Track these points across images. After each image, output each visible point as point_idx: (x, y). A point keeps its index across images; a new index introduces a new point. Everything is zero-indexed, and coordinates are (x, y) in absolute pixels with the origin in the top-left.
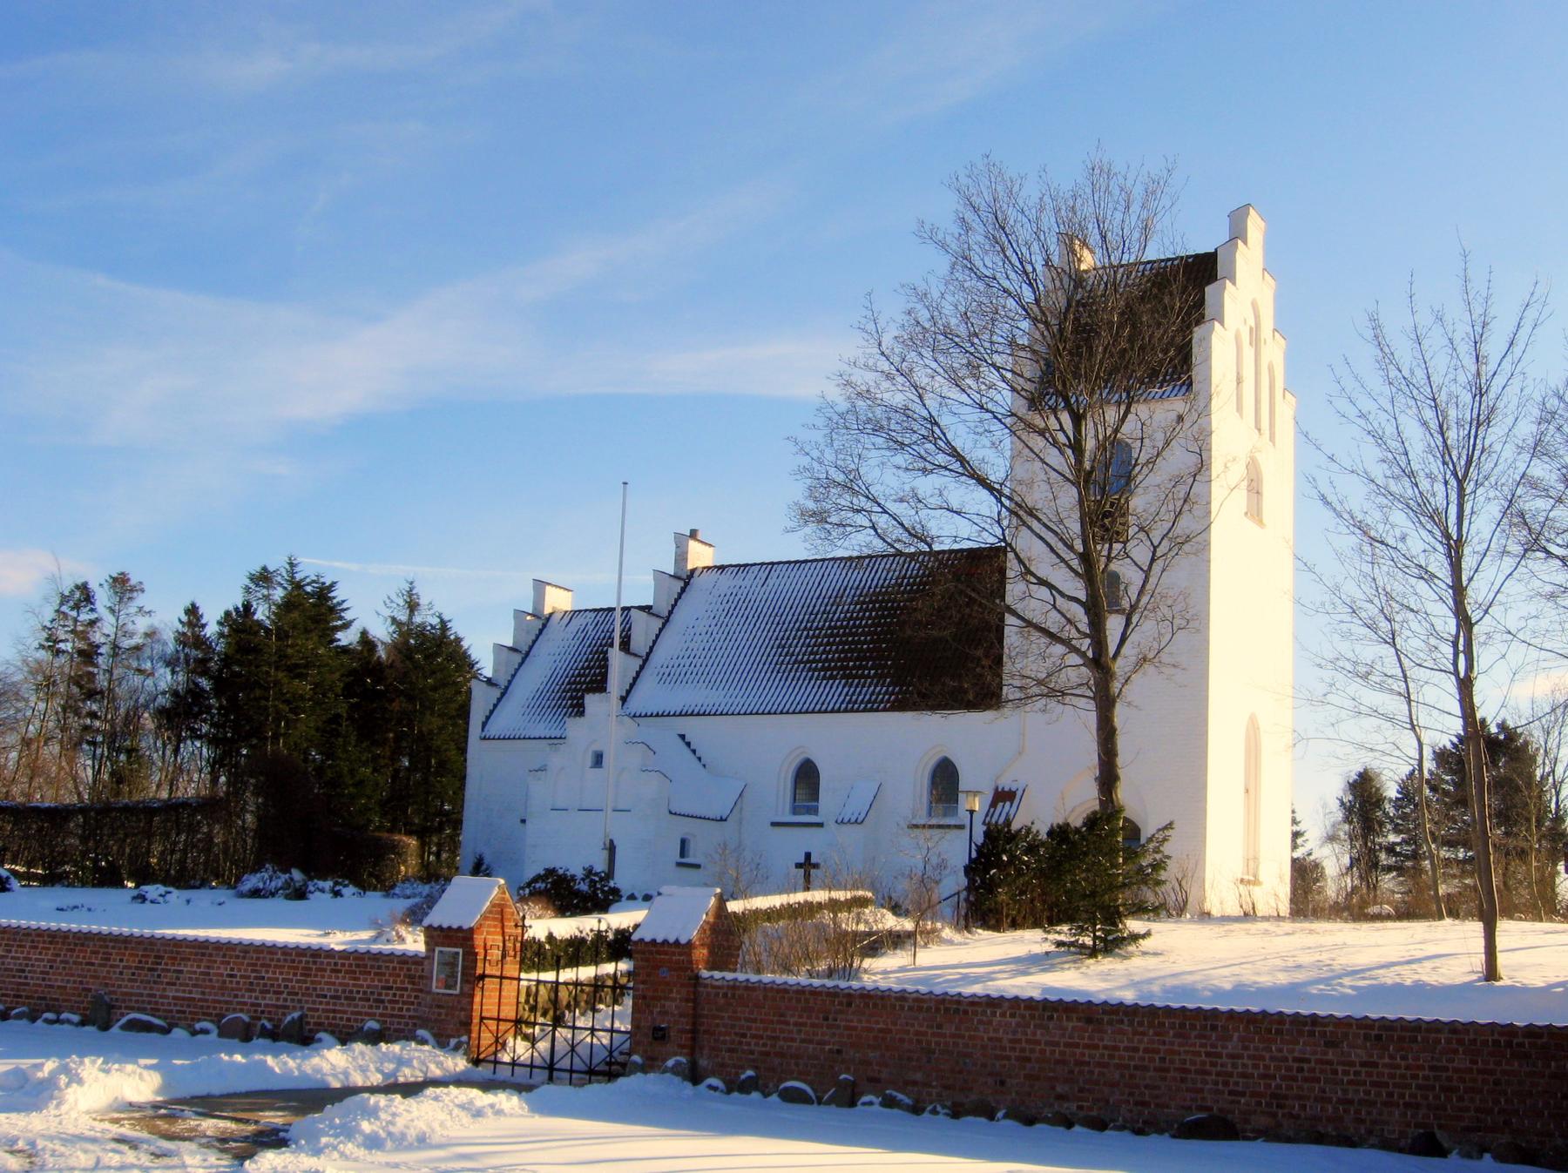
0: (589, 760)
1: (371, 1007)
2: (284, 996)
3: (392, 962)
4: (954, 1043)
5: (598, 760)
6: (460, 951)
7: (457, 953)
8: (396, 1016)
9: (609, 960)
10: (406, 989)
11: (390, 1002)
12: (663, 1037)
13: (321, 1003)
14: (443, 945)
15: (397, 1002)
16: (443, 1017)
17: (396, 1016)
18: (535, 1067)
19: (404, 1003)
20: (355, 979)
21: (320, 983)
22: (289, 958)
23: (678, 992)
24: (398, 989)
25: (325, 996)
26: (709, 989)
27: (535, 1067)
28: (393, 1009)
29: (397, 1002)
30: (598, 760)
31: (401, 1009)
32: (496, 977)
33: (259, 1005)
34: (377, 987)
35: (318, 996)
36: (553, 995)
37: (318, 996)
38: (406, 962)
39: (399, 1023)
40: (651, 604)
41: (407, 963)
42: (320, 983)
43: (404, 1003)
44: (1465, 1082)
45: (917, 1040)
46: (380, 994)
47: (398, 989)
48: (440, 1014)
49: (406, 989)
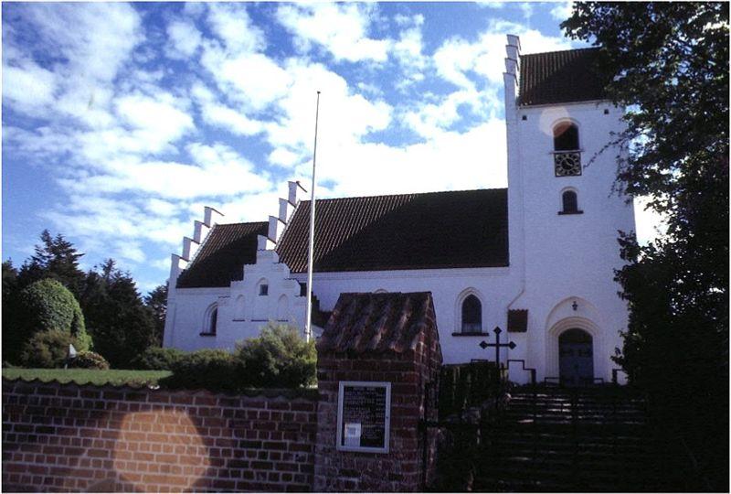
0: (258, 290)
2: (85, 456)
4: (273, 413)
5: (264, 290)
6: (388, 386)
7: (383, 390)
10: (283, 446)
13: (142, 467)
15: (269, 466)
18: (501, 345)
20: (42, 420)
21: (142, 437)
22: (93, 400)
24: (269, 446)
25: (149, 457)
27: (501, 345)
30: (264, 290)
33: (43, 470)
35: (138, 456)
36: (227, 7)
37: (138, 456)
40: (501, 182)
42: (142, 437)
44: (207, 414)
45: (86, 403)
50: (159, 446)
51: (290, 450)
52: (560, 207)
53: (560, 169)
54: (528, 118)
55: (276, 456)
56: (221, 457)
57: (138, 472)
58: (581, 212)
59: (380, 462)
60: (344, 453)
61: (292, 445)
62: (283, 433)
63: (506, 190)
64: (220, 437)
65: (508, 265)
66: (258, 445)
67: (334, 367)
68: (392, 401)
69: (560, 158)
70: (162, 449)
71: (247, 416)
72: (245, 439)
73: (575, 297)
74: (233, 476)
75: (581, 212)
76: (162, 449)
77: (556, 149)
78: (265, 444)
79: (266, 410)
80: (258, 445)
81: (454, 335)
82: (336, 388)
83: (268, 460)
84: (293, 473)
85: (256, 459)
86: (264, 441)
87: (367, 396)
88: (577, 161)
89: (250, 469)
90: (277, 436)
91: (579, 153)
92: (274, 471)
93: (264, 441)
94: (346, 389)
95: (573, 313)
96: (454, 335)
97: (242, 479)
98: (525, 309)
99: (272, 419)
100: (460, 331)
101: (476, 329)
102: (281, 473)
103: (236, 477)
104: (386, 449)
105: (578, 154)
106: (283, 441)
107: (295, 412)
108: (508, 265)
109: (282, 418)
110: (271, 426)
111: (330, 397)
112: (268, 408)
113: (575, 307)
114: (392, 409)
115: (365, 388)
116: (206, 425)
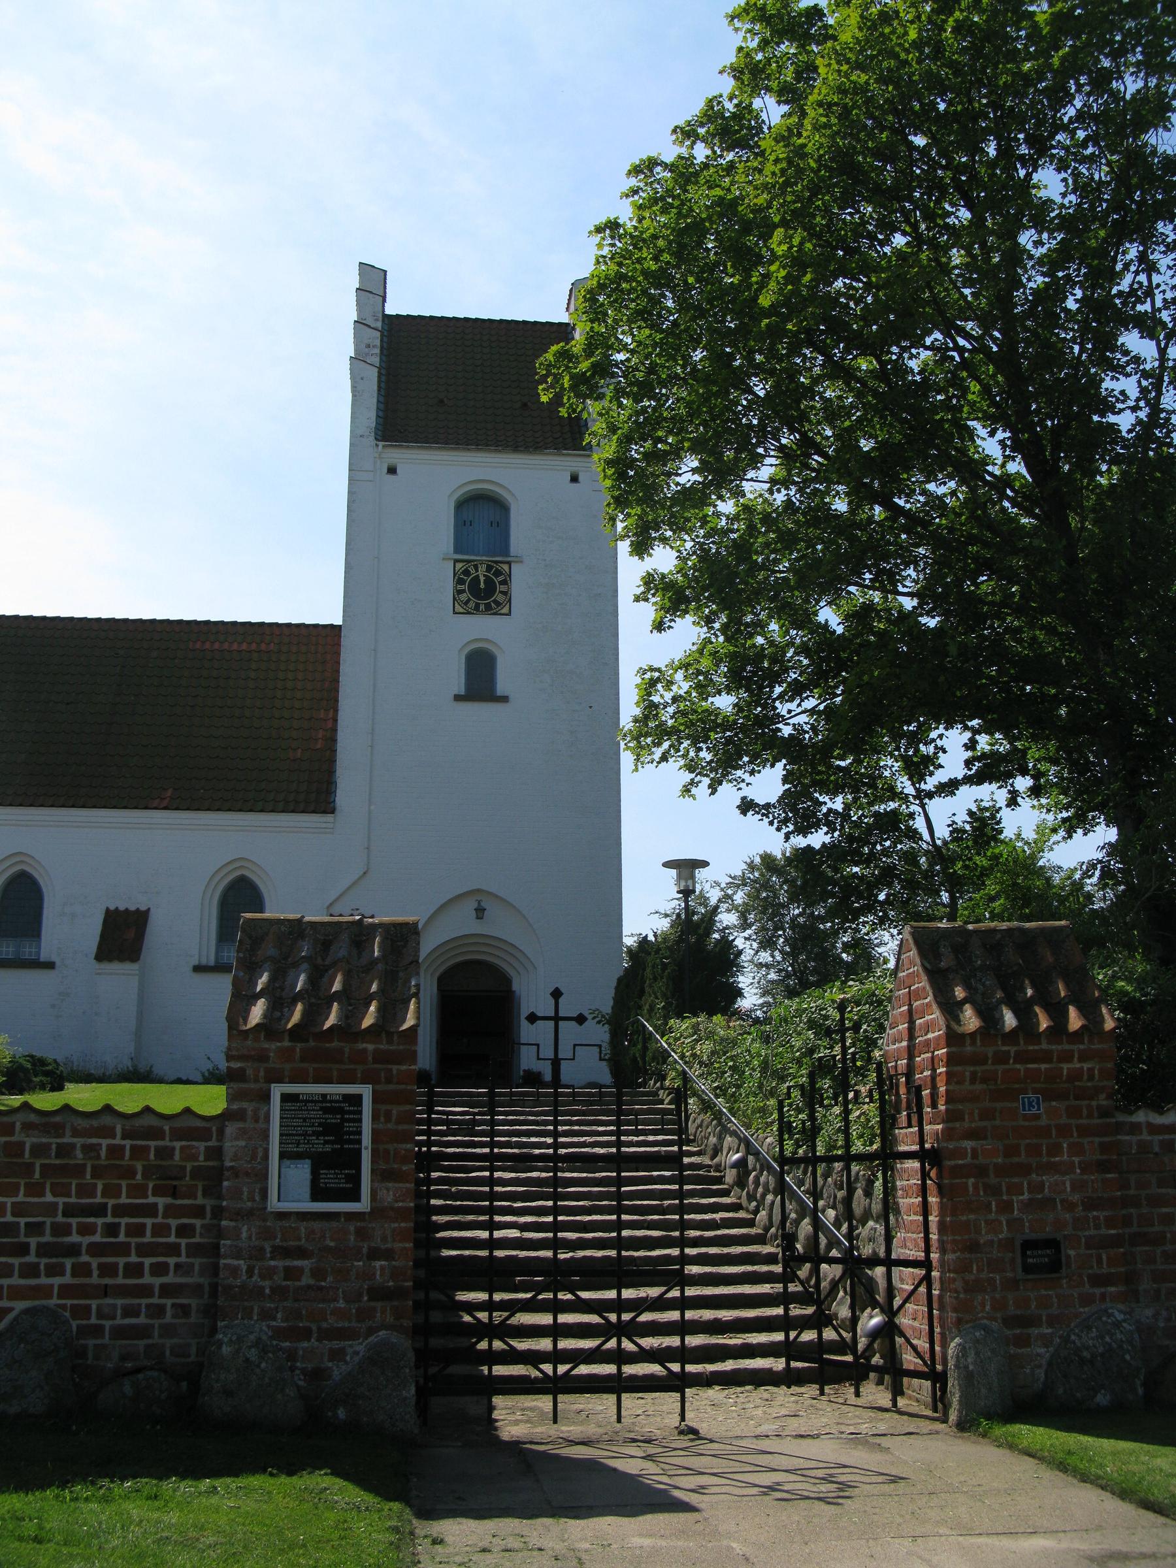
1: (31, 1271)
3: (109, 1132)
6: (366, 1091)
7: (357, 1099)
8: (123, 1291)
9: (947, 1091)
10: (151, 1211)
11: (96, 1250)
12: (1055, 1266)
14: (299, 1077)
15: (124, 1249)
16: (306, 1280)
17: (123, 1291)
19: (143, 1250)
20: (174, 1193)
23: (1077, 1149)
24: (120, 1211)
26: (1145, 1137)
28: (108, 1270)
29: (124, 1249)
31: (112, 1230)
32: (889, 1250)
34: (51, 1209)
38: (156, 1134)
39: (129, 1312)
40: (338, 621)
41: (156, 1134)
43: (143, 1250)
46: (61, 1230)
47: (120, 1211)
48: (290, 1274)
49: (151, 1211)
50: (41, 1225)
51: (165, 1216)
52: (458, 684)
53: (464, 597)
54: (581, 478)
55: (139, 1230)
56: (23, 1239)
57: (44, 1280)
58: (504, 699)
59: (352, 1228)
60: (282, 1216)
61: (167, 1207)
62: (151, 1185)
63: (333, 631)
64: (21, 1198)
65: (333, 811)
66: (100, 1211)
67: (262, 1057)
68: (375, 1117)
69: (466, 572)
70: (48, 1231)
71: (79, 1154)
72: (73, 1200)
73: (479, 891)
74: (47, 1276)
75: (504, 699)
76: (48, 1231)
77: (458, 549)
78: (115, 1207)
79: (118, 1141)
80: (100, 1211)
81: (198, 969)
82: (266, 1097)
83: (122, 1238)
84: (172, 1261)
85: (97, 1238)
86: (111, 1202)
87: (325, 1110)
88: (504, 582)
89: (85, 1258)
90: (138, 1190)
91: (509, 563)
92: (134, 1259)
93: (111, 1202)
94: (286, 1098)
95: (474, 927)
96: (198, 969)
97: (67, 1279)
98: (143, 908)
99: (131, 1158)
100: (212, 963)
101: (28, 951)
102: (148, 1261)
103: (54, 1275)
104: (363, 1205)
105: (506, 567)
106: (151, 1200)
107: (178, 1145)
108: (333, 811)
109: (152, 1156)
110: (130, 1173)
111: (250, 1113)
112: (124, 1138)
113: (480, 912)
114: (375, 1134)
115: (324, 1096)
116: (93, 1177)
